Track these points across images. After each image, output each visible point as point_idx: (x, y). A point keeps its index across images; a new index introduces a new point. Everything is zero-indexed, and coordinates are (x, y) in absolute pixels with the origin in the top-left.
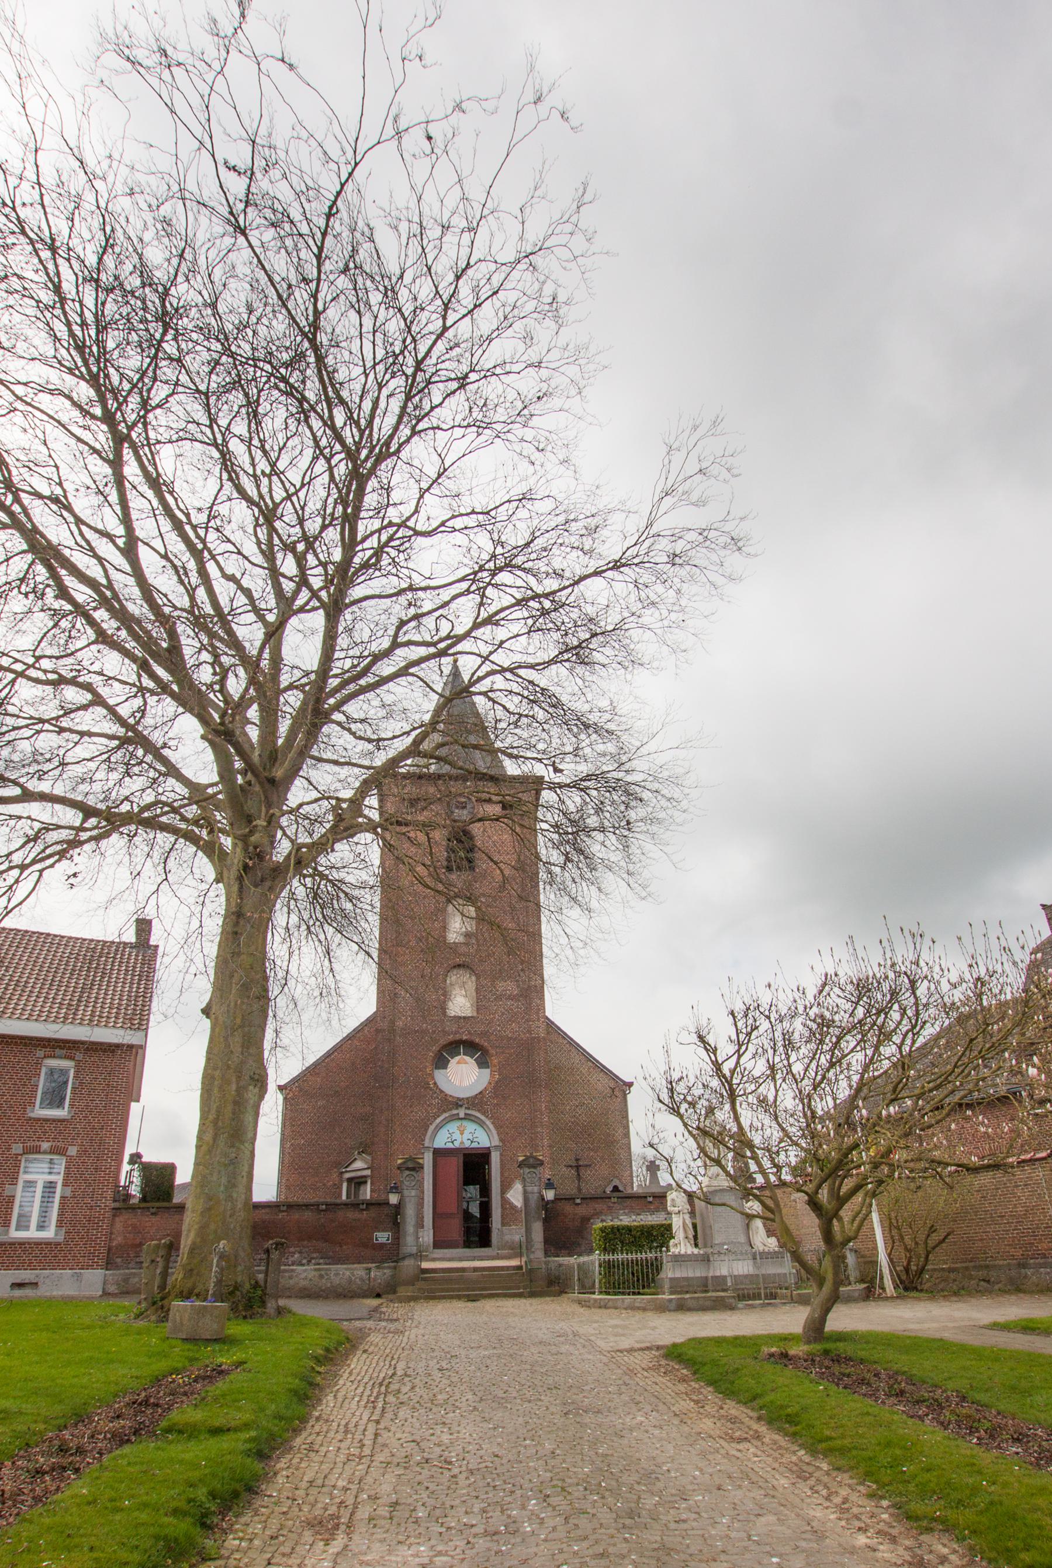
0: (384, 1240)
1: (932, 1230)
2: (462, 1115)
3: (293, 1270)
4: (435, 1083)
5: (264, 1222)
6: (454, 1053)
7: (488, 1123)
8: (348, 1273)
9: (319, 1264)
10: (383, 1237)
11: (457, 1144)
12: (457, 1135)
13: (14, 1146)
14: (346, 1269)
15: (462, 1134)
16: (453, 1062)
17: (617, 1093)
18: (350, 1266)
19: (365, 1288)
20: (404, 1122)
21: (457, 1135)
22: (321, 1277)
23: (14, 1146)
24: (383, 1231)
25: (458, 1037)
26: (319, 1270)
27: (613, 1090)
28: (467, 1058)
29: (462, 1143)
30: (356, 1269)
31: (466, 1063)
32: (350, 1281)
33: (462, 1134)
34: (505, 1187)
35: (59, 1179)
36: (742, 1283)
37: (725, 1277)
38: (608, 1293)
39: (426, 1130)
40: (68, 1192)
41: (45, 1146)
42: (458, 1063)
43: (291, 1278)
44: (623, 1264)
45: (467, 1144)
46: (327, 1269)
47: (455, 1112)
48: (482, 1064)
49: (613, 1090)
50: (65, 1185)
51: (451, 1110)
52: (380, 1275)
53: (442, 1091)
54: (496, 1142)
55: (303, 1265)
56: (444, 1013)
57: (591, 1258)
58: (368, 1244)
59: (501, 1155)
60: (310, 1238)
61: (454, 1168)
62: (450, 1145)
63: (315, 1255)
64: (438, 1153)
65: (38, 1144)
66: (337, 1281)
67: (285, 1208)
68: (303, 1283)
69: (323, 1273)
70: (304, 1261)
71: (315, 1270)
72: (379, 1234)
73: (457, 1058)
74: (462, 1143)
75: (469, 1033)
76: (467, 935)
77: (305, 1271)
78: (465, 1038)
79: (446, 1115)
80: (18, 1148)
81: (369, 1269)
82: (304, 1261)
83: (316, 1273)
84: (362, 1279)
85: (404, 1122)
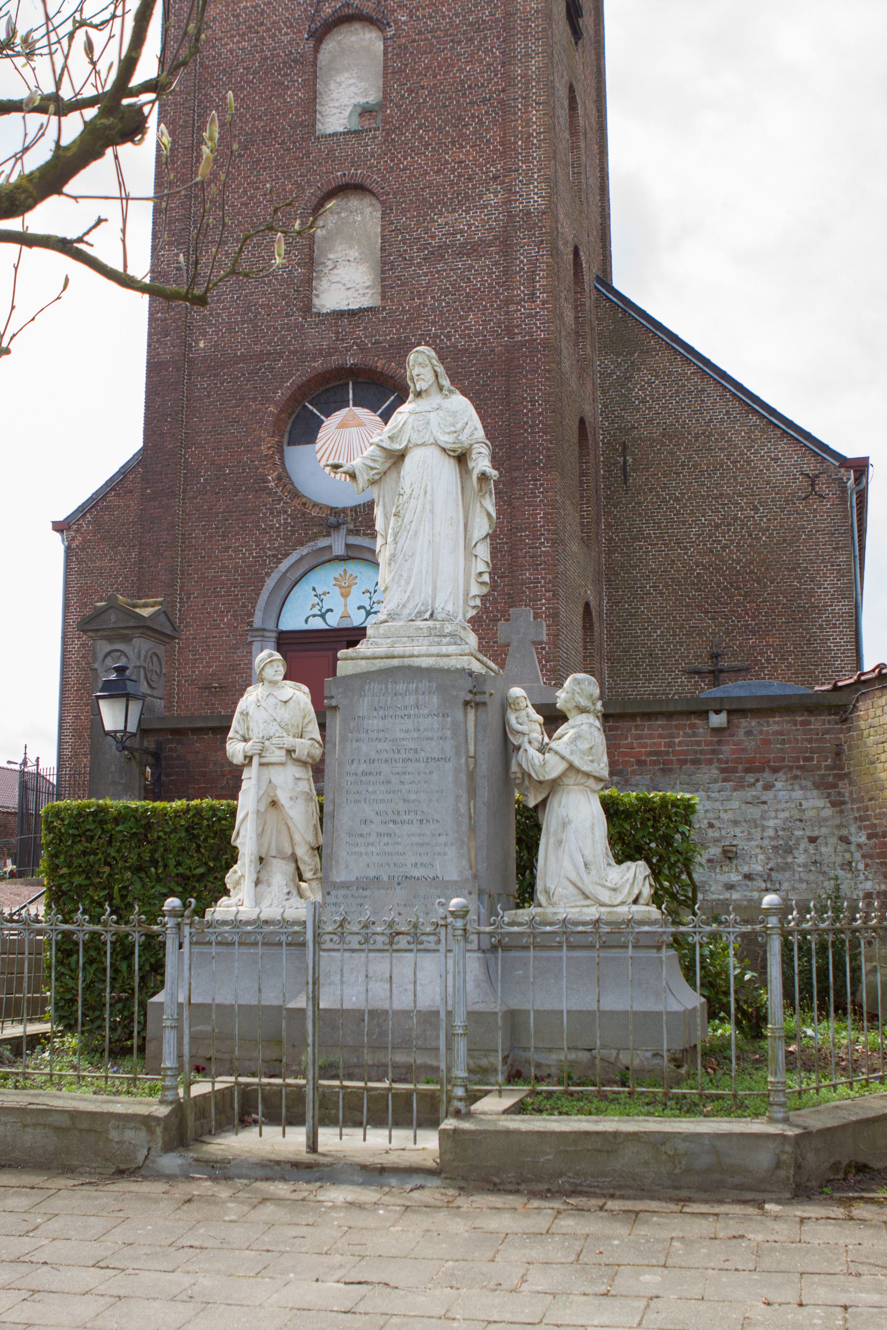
1: (304, 717)
2: (339, 549)
6: (337, 404)
11: (333, 621)
12: (334, 600)
15: (345, 595)
16: (331, 425)
17: (822, 487)
20: (210, 574)
25: (334, 361)
27: (813, 480)
28: (362, 413)
33: (345, 595)
36: (405, 1044)
37: (529, 1011)
39: (258, 592)
42: (342, 425)
44: (822, 949)
47: (323, 542)
49: (813, 480)
51: (314, 538)
56: (307, 308)
62: (317, 624)
75: (362, 348)
76: (365, 111)
78: (350, 361)
79: (304, 551)
85: (210, 574)
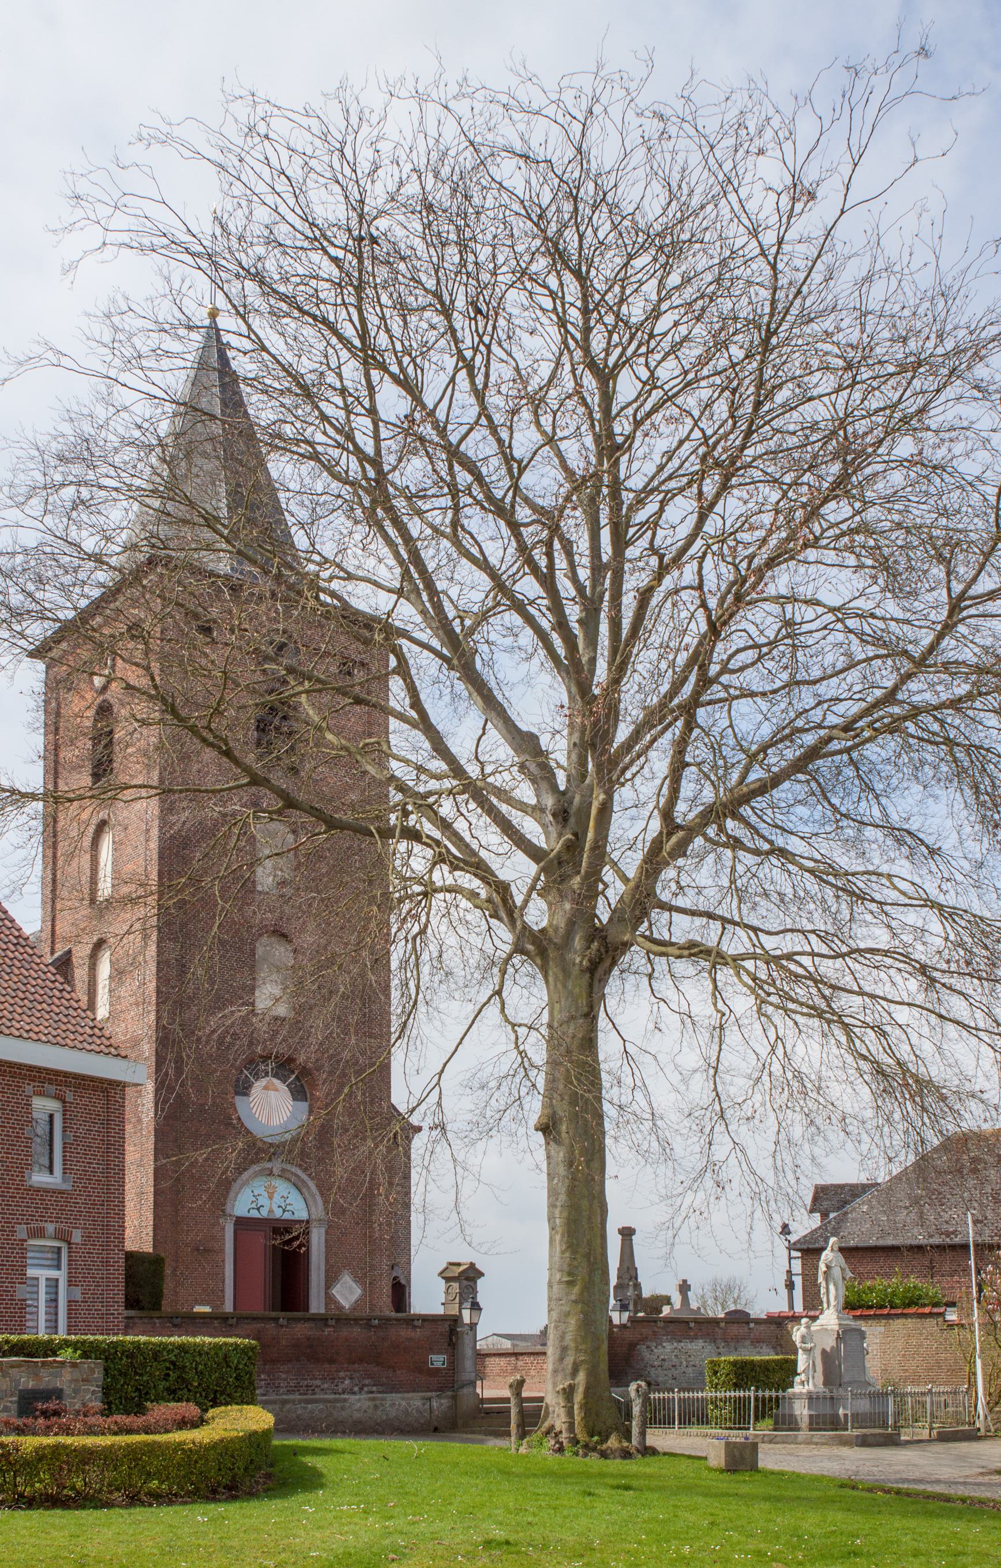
0: (438, 1365)
3: (345, 1400)
4: (239, 1119)
5: (308, 1339)
7: (312, 1185)
8: (404, 1403)
9: (372, 1392)
10: (438, 1360)
11: (264, 1213)
13: (18, 1227)
14: (403, 1399)
15: (271, 1198)
16: (258, 1086)
18: (406, 1395)
19: (422, 1421)
21: (263, 1200)
22: (376, 1407)
23: (18, 1227)
24: (438, 1353)
26: (373, 1399)
28: (277, 1082)
29: (271, 1211)
30: (412, 1399)
31: (276, 1090)
32: (407, 1413)
33: (271, 1198)
34: (331, 1279)
35: (61, 1275)
38: (775, 1430)
40: (78, 1294)
41: (50, 1228)
42: (266, 1088)
43: (343, 1408)
45: (278, 1213)
46: (382, 1399)
48: (299, 1093)
50: (70, 1283)
52: (440, 1404)
53: (248, 1132)
54: (319, 1211)
55: (354, 1393)
57: (747, 1393)
58: (422, 1368)
59: (327, 1233)
60: (361, 1361)
61: (260, 1243)
62: (254, 1214)
63: (367, 1382)
64: (243, 1224)
65: (42, 1224)
66: (393, 1413)
67: (333, 1322)
68: (357, 1415)
69: (378, 1402)
70: (356, 1389)
71: (370, 1399)
72: (434, 1357)
73: (263, 1082)
74: (271, 1211)
77: (359, 1400)
80: (21, 1231)
81: (429, 1399)
82: (356, 1389)
83: (371, 1403)
84: (418, 1410)
